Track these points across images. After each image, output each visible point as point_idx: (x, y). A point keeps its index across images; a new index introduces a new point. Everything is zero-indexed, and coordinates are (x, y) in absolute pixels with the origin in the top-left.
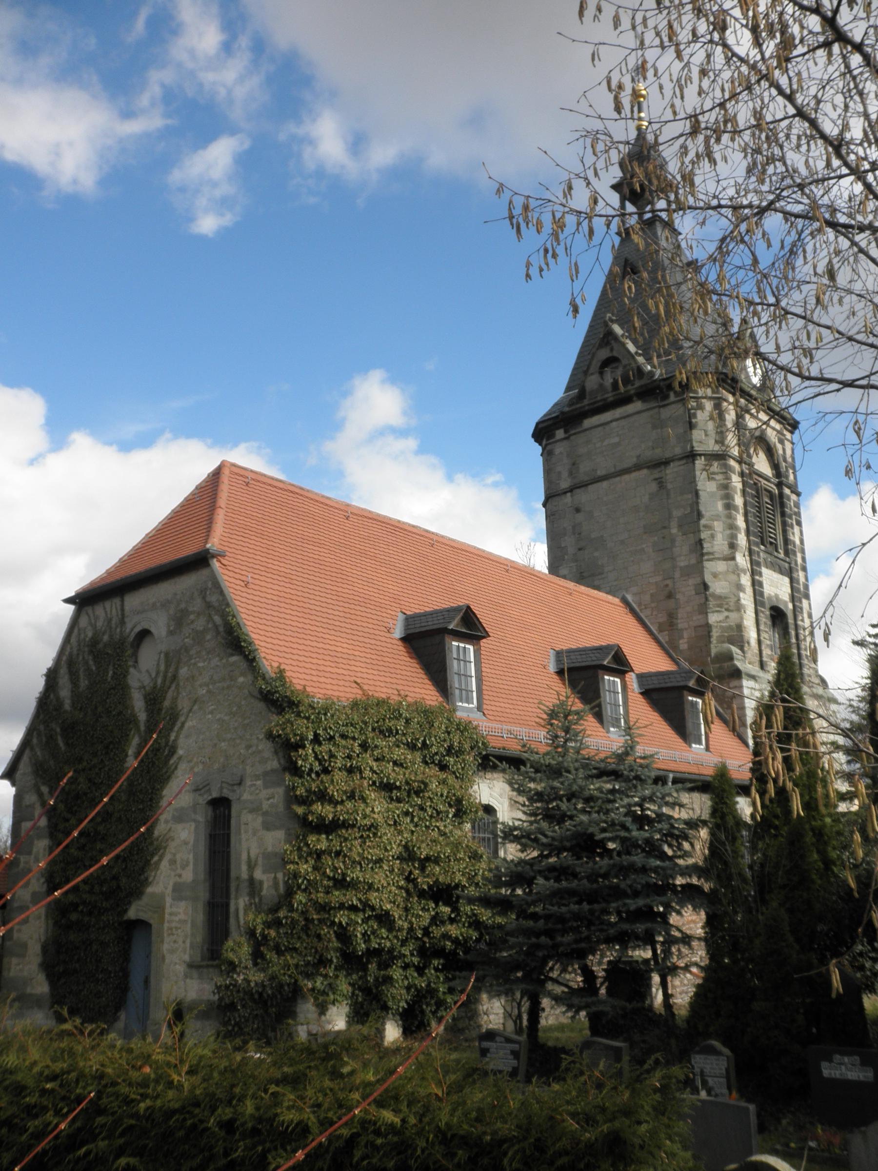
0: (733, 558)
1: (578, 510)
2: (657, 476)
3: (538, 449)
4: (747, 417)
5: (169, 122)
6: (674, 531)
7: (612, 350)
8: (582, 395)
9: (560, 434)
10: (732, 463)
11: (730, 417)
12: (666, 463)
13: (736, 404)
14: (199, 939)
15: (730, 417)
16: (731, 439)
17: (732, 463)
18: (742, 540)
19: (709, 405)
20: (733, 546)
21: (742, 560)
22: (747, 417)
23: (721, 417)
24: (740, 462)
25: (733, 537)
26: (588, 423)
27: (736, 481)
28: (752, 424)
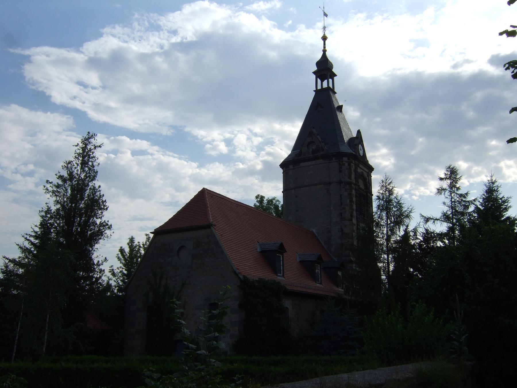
0: (352, 220)
1: (297, 197)
2: (228, 135)
3: (282, 171)
4: (358, 168)
5: (18, 51)
6: (332, 208)
7: (312, 138)
8: (300, 153)
9: (291, 167)
10: (353, 185)
11: (353, 169)
12: (330, 183)
13: (355, 164)
14: (67, 106)
15: (353, 169)
16: (353, 177)
17: (353, 185)
18: (355, 214)
19: (347, 164)
20: (352, 216)
21: (354, 221)
22: (358, 168)
23: (350, 169)
24: (355, 185)
25: (352, 212)
26: (303, 164)
27: (354, 192)
28: (359, 170)
